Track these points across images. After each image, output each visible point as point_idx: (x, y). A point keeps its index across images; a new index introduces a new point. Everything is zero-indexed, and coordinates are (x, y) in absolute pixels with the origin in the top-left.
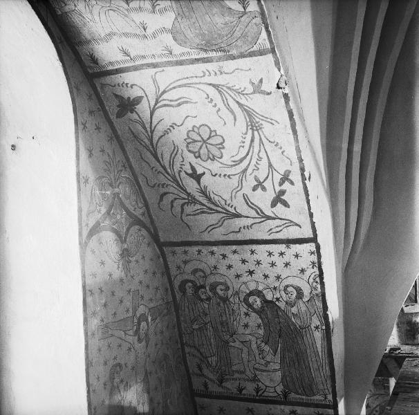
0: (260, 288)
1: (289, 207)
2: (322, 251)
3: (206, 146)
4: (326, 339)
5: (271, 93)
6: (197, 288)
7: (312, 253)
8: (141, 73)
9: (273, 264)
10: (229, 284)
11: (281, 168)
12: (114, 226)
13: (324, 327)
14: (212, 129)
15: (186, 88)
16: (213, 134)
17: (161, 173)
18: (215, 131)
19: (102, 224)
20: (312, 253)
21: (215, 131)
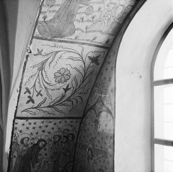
0: (40, 138)
1: (27, 103)
2: (12, 123)
3: (64, 77)
4: (4, 127)
5: (43, 49)
6: (67, 137)
7: (16, 124)
8: (89, 47)
9: (34, 128)
10: (53, 135)
11: (112, 89)
12: (101, 110)
13: (11, 157)
14: (57, 72)
15: (52, 63)
16: (59, 72)
17: (74, 89)
18: (58, 71)
19: (31, 95)
20: (16, 124)
21: (58, 71)
